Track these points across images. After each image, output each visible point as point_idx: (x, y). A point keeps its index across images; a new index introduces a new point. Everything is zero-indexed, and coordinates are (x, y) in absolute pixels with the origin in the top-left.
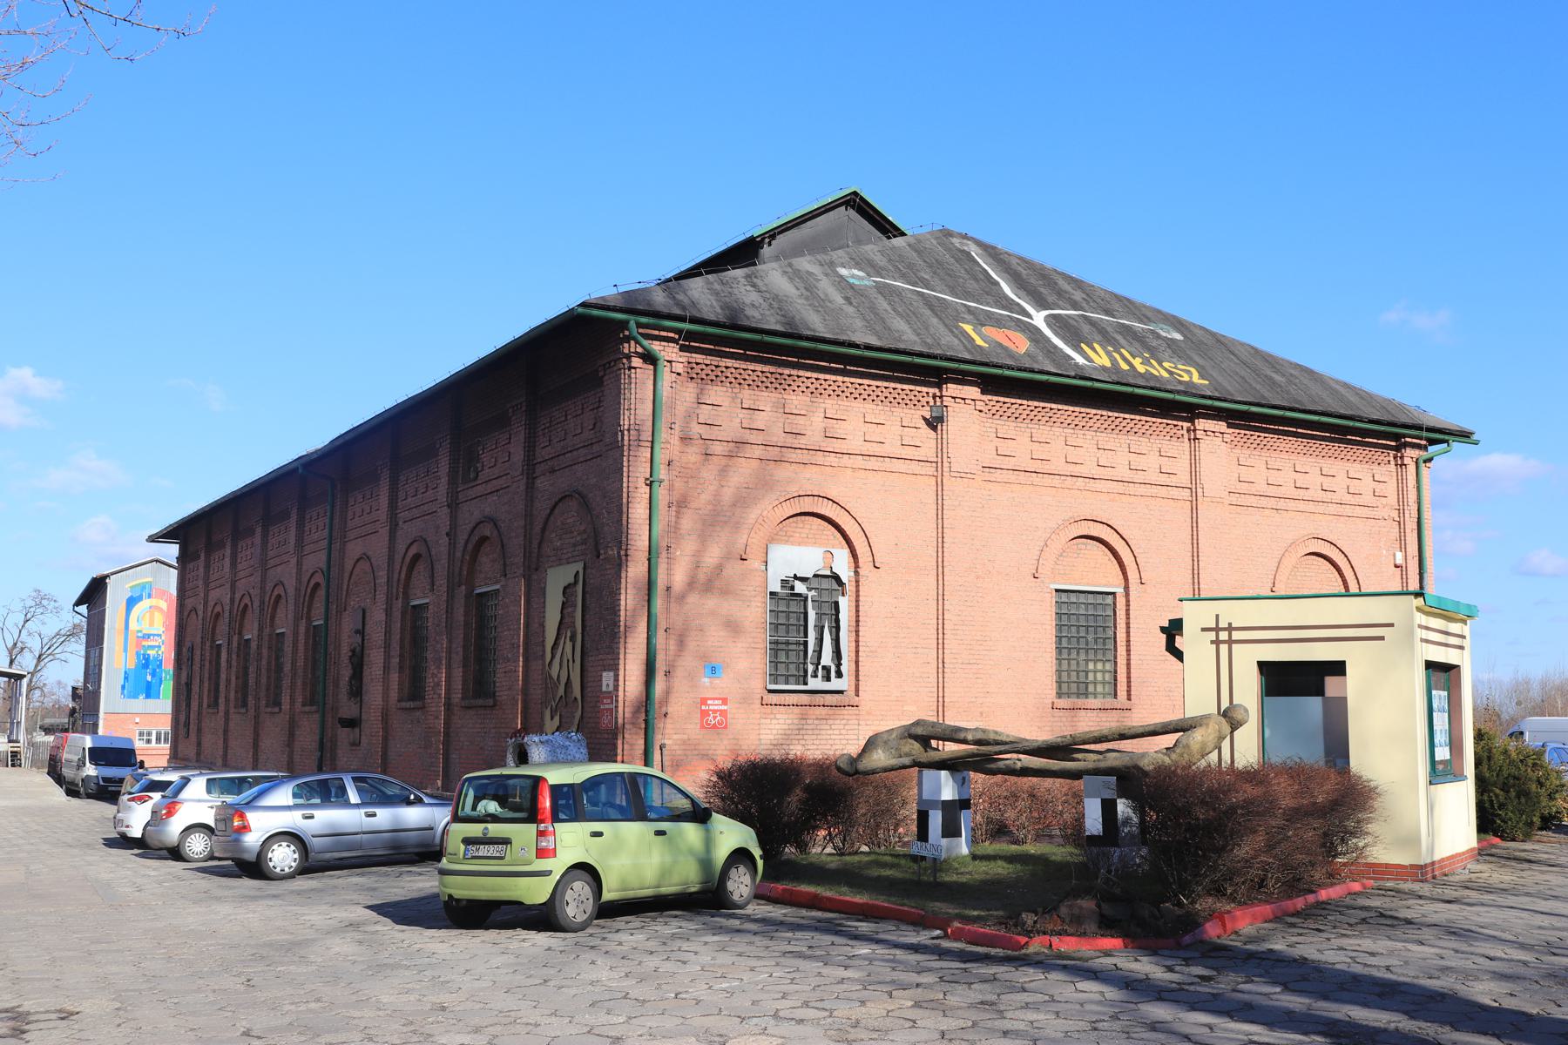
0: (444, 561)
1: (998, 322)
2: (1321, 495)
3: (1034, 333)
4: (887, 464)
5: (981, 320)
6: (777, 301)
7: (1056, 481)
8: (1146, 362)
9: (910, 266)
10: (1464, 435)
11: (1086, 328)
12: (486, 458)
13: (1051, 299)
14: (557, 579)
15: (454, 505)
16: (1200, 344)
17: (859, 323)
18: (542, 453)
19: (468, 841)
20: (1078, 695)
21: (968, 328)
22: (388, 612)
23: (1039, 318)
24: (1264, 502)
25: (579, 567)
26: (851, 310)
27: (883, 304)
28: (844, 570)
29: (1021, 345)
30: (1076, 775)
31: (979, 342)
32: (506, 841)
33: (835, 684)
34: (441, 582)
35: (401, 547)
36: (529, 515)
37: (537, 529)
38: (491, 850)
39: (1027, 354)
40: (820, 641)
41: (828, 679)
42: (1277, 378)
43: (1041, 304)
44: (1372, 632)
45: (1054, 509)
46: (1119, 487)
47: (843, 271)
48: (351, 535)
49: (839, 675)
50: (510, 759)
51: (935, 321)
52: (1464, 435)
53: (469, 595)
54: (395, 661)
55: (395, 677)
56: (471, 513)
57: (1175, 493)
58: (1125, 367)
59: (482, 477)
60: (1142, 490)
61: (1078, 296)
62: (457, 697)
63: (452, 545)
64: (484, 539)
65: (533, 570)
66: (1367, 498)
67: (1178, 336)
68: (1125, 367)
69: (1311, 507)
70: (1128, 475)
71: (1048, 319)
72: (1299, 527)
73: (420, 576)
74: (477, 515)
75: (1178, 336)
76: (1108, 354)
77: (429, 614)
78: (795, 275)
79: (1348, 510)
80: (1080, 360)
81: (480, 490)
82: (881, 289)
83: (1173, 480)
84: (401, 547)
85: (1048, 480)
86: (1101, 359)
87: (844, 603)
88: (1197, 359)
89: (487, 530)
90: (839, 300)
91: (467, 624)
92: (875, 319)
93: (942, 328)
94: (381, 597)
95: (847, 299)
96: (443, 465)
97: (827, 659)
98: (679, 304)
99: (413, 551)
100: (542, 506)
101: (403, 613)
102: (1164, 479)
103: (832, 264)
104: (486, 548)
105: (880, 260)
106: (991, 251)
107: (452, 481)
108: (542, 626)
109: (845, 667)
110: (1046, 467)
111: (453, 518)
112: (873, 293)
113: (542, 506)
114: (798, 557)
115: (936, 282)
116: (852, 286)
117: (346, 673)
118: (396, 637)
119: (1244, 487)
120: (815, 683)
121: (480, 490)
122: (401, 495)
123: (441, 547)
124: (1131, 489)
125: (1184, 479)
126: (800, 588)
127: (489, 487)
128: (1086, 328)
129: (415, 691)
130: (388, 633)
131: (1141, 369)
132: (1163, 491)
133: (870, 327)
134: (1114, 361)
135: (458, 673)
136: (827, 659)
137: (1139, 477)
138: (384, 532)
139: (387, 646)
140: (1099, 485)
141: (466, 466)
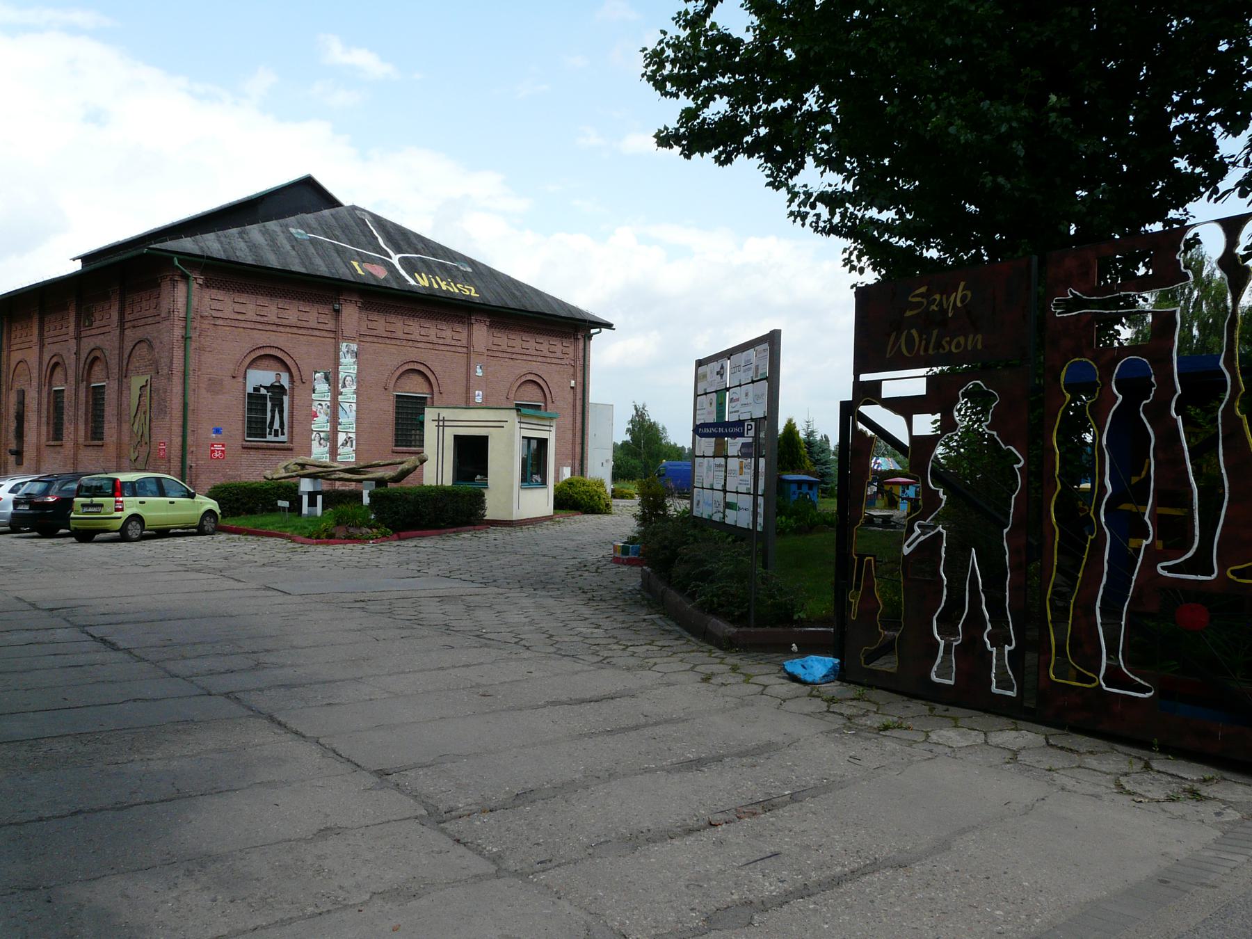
0: (73, 367)
1: (372, 260)
2: (535, 353)
3: (391, 267)
4: (310, 332)
5: (363, 259)
6: (253, 247)
7: (398, 342)
8: (448, 284)
9: (330, 227)
10: (609, 326)
11: (420, 264)
12: (97, 315)
13: (405, 247)
14: (137, 382)
15: (78, 338)
16: (481, 273)
17: (297, 261)
18: (128, 317)
19: (84, 505)
20: (169, 461)
21: (355, 264)
22: (40, 392)
23: (395, 259)
24: (505, 355)
25: (148, 377)
26: (293, 253)
27: (312, 250)
28: (285, 381)
29: (381, 273)
30: (360, 481)
31: (360, 272)
32: (101, 505)
33: (281, 438)
34: (72, 379)
35: (46, 358)
36: (121, 348)
37: (126, 356)
38: (94, 510)
39: (385, 279)
40: (273, 417)
41: (276, 435)
42: (517, 293)
43: (398, 250)
44: (499, 424)
45: (392, 358)
46: (431, 346)
47: (293, 230)
48: (14, 348)
49: (283, 434)
50: (1141, 508)
51: (338, 259)
52: (609, 326)
53: (87, 387)
54: (44, 420)
55: (44, 429)
56: (88, 344)
57: (459, 349)
58: (436, 286)
59: (94, 325)
60: (442, 348)
61: (420, 246)
62: (81, 440)
63: (78, 359)
64: (96, 358)
65: (124, 375)
66: (559, 355)
67: (469, 270)
68: (436, 286)
69: (529, 358)
70: (435, 340)
71: (400, 260)
72: (522, 368)
73: (59, 373)
74: (92, 346)
75: (469, 270)
76: (429, 279)
77: (66, 394)
78: (265, 232)
79: (549, 360)
80: (412, 282)
81: (93, 332)
82: (312, 241)
83: (459, 343)
84: (46, 358)
85: (393, 342)
86: (424, 282)
87: (286, 399)
88: (477, 282)
89: (97, 353)
90: (288, 247)
91: (87, 402)
92: (304, 258)
93: (342, 264)
94: (35, 383)
95: (293, 247)
96: (72, 319)
97: (276, 426)
98: (201, 248)
99: (54, 360)
100: (128, 346)
101: (49, 394)
102: (454, 343)
103: (287, 226)
104: (98, 363)
105: (314, 224)
106: (379, 222)
107: (78, 325)
108: (129, 405)
109: (286, 431)
110: (393, 335)
111: (78, 345)
112: (307, 243)
113: (128, 346)
114: (262, 377)
115: (342, 237)
116: (296, 239)
117: (13, 425)
118: (45, 407)
119: (495, 348)
120: (270, 438)
121: (93, 332)
122: (46, 329)
123: (70, 360)
124: (437, 347)
125: (464, 343)
126: (263, 391)
127: (99, 331)
128: (420, 264)
129: (57, 434)
130: (39, 404)
131: (444, 288)
132: (453, 349)
133: (303, 264)
134: (431, 283)
135: (82, 427)
136: (276, 426)
137: (441, 341)
138: (36, 349)
139: (39, 411)
140: (420, 345)
141: (85, 318)
